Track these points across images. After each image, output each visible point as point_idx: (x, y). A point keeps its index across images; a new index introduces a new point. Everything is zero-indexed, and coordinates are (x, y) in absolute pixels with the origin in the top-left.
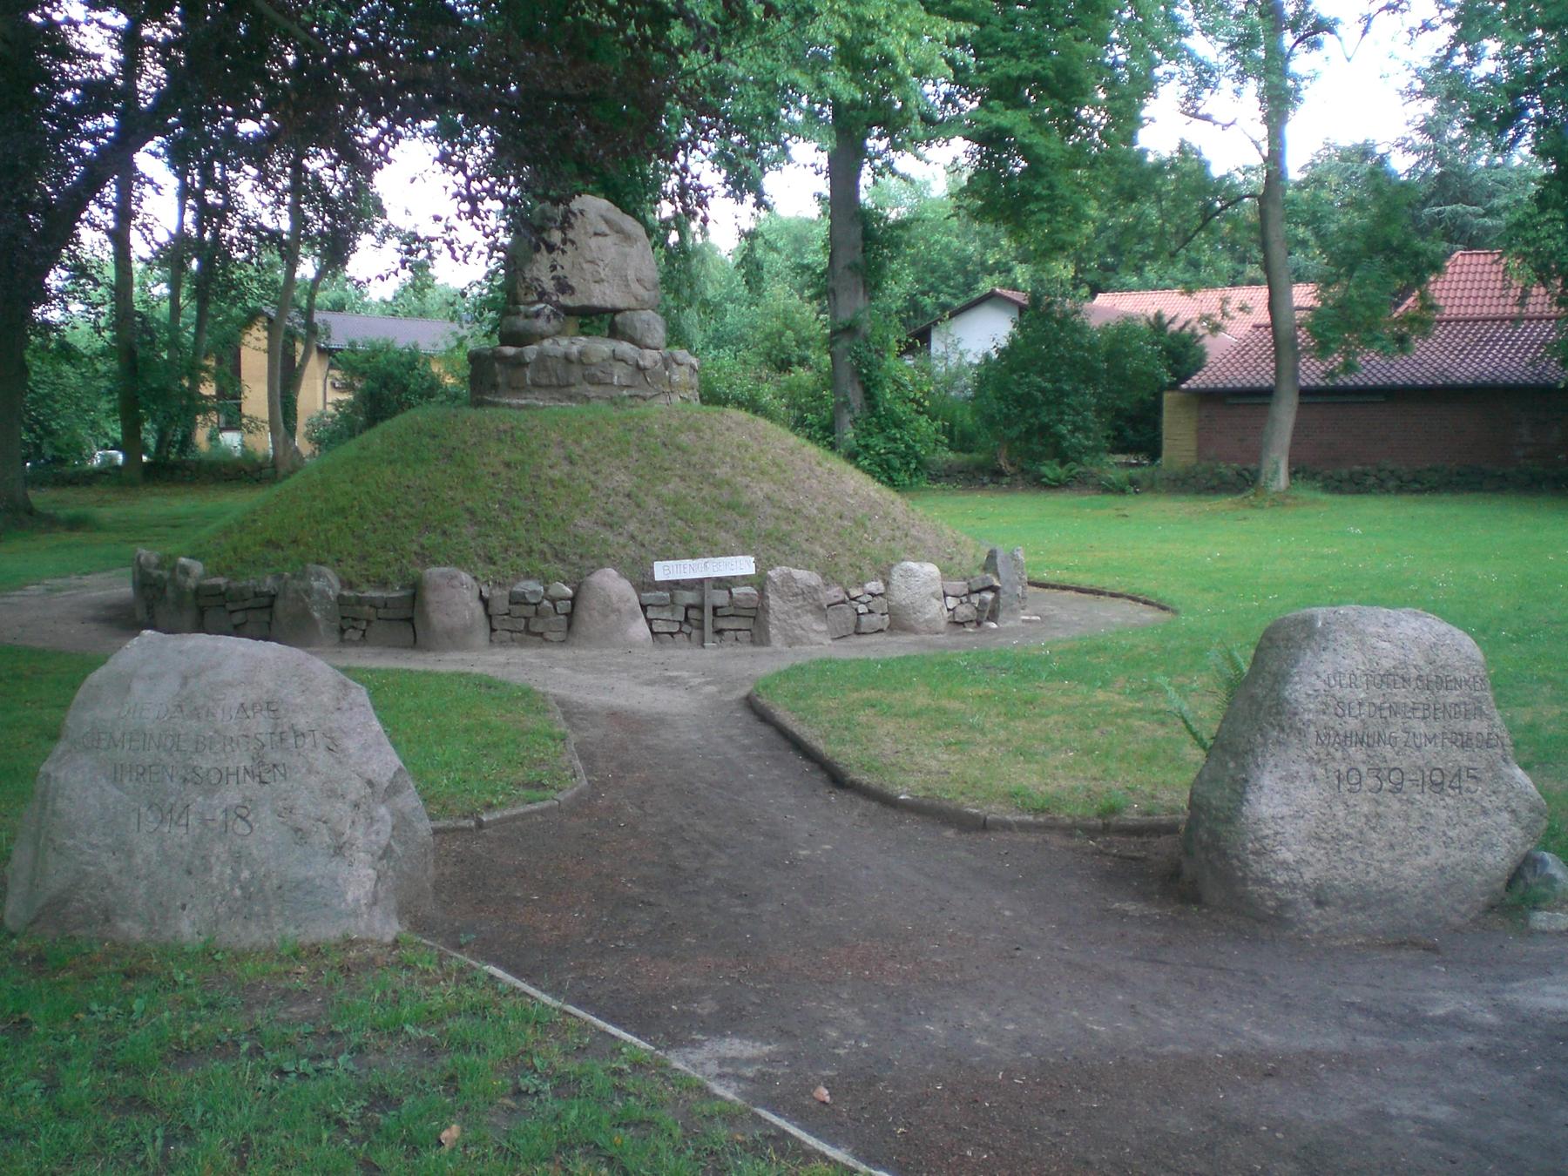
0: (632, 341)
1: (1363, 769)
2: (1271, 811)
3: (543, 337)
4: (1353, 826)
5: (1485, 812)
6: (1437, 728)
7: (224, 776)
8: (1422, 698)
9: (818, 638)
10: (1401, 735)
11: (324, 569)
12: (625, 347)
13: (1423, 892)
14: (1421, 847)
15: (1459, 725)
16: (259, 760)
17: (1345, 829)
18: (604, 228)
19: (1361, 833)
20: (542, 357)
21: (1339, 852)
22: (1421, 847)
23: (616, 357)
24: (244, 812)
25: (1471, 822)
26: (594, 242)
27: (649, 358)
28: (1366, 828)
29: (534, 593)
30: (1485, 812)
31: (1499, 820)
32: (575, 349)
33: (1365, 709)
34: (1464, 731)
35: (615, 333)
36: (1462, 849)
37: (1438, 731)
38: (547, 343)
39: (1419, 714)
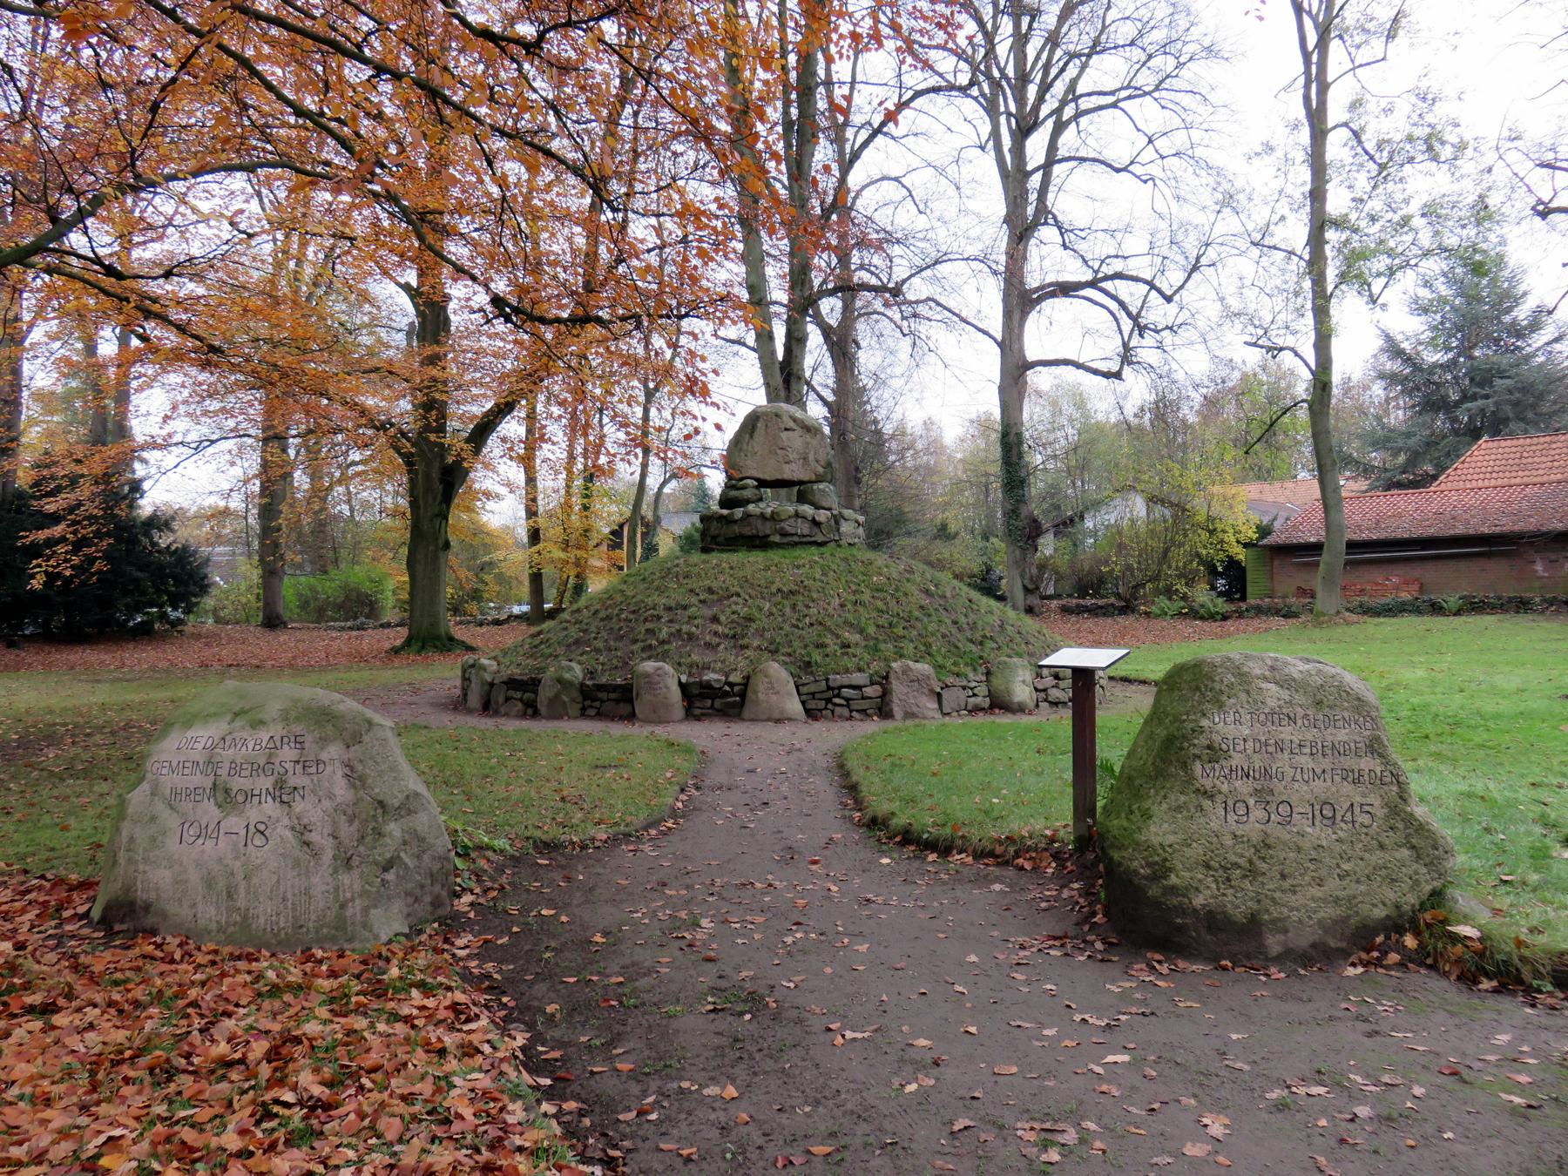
0: (812, 504)
1: (1251, 802)
2: (1160, 839)
3: (748, 502)
4: (1242, 856)
5: (1382, 847)
6: (1326, 763)
7: (249, 795)
8: (1309, 737)
9: (931, 714)
10: (1290, 772)
11: (573, 664)
12: (807, 509)
13: (1320, 922)
14: (1313, 878)
15: (1348, 762)
16: (280, 784)
17: (1234, 859)
18: (791, 424)
19: (1251, 862)
20: (747, 516)
21: (1229, 880)
22: (1313, 878)
23: (797, 515)
24: (262, 827)
25: (1367, 856)
26: (785, 435)
27: (822, 516)
28: (1255, 858)
29: (718, 681)
30: (1382, 847)
31: (1398, 855)
32: (769, 510)
33: (1250, 744)
34: (1356, 768)
35: (802, 498)
36: (1358, 882)
37: (1328, 767)
38: (751, 507)
39: (1307, 750)
